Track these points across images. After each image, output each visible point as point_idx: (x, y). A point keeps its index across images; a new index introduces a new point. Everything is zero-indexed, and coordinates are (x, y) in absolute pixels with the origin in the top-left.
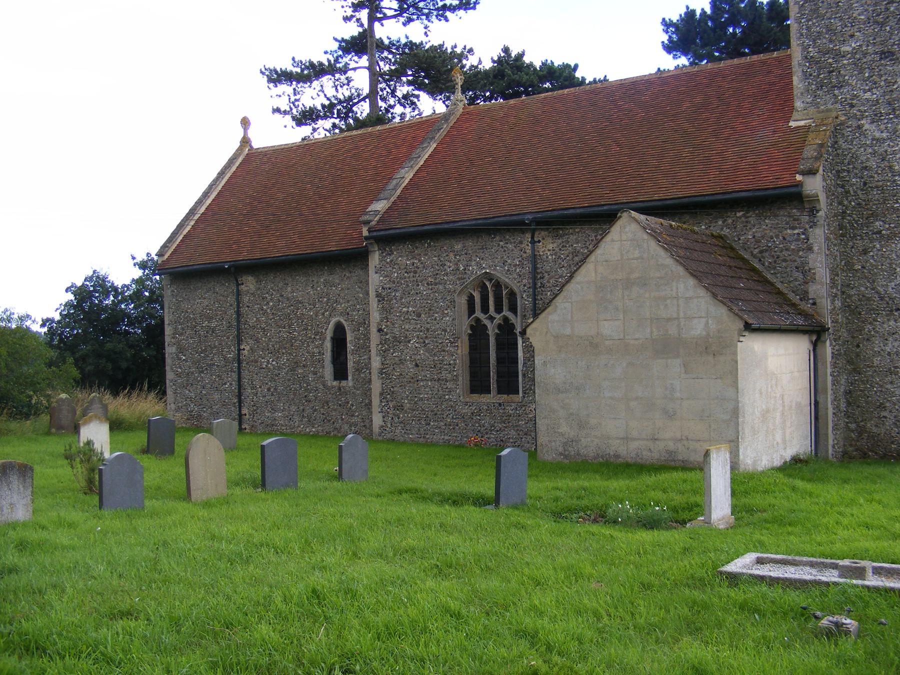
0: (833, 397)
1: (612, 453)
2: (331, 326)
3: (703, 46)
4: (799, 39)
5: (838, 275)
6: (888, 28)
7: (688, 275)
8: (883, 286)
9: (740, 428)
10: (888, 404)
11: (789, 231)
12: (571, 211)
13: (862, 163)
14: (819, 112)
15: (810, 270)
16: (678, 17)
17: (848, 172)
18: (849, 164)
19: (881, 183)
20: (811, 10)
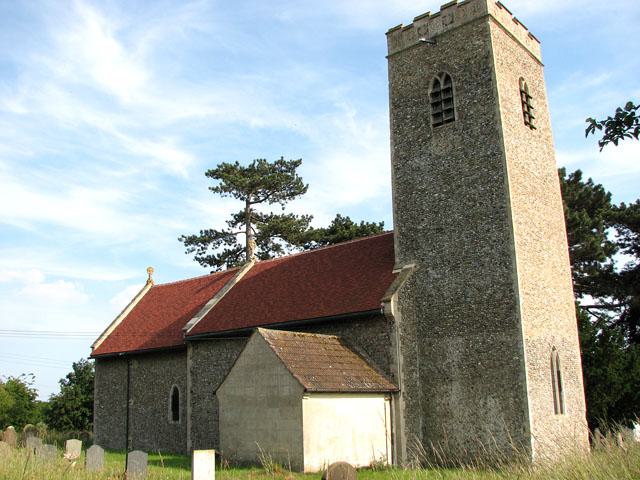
2: (172, 389)
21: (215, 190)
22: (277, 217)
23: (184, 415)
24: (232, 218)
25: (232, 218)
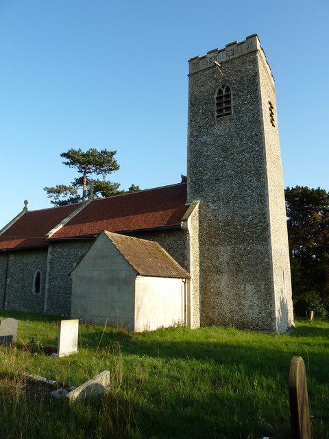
21: (67, 164)
22: (100, 182)
23: (44, 289)
24: (75, 181)
25: (75, 181)
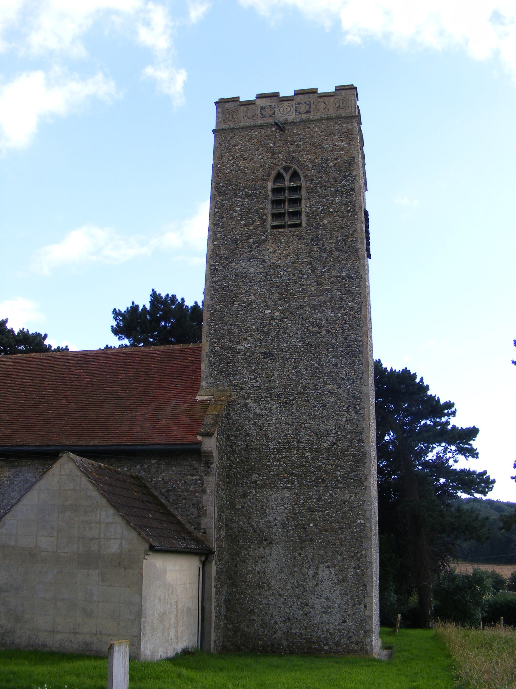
0: (216, 604)
1: (40, 643)
3: (141, 334)
4: (208, 337)
5: (224, 513)
6: (270, 337)
7: (109, 505)
8: (256, 522)
9: (142, 627)
10: (256, 611)
11: (189, 477)
12: (26, 448)
13: (246, 431)
14: (218, 391)
15: (203, 507)
16: (125, 309)
17: (236, 436)
18: (236, 431)
19: (258, 447)
20: (219, 317)
